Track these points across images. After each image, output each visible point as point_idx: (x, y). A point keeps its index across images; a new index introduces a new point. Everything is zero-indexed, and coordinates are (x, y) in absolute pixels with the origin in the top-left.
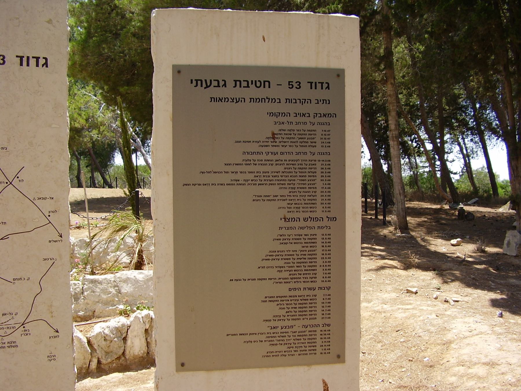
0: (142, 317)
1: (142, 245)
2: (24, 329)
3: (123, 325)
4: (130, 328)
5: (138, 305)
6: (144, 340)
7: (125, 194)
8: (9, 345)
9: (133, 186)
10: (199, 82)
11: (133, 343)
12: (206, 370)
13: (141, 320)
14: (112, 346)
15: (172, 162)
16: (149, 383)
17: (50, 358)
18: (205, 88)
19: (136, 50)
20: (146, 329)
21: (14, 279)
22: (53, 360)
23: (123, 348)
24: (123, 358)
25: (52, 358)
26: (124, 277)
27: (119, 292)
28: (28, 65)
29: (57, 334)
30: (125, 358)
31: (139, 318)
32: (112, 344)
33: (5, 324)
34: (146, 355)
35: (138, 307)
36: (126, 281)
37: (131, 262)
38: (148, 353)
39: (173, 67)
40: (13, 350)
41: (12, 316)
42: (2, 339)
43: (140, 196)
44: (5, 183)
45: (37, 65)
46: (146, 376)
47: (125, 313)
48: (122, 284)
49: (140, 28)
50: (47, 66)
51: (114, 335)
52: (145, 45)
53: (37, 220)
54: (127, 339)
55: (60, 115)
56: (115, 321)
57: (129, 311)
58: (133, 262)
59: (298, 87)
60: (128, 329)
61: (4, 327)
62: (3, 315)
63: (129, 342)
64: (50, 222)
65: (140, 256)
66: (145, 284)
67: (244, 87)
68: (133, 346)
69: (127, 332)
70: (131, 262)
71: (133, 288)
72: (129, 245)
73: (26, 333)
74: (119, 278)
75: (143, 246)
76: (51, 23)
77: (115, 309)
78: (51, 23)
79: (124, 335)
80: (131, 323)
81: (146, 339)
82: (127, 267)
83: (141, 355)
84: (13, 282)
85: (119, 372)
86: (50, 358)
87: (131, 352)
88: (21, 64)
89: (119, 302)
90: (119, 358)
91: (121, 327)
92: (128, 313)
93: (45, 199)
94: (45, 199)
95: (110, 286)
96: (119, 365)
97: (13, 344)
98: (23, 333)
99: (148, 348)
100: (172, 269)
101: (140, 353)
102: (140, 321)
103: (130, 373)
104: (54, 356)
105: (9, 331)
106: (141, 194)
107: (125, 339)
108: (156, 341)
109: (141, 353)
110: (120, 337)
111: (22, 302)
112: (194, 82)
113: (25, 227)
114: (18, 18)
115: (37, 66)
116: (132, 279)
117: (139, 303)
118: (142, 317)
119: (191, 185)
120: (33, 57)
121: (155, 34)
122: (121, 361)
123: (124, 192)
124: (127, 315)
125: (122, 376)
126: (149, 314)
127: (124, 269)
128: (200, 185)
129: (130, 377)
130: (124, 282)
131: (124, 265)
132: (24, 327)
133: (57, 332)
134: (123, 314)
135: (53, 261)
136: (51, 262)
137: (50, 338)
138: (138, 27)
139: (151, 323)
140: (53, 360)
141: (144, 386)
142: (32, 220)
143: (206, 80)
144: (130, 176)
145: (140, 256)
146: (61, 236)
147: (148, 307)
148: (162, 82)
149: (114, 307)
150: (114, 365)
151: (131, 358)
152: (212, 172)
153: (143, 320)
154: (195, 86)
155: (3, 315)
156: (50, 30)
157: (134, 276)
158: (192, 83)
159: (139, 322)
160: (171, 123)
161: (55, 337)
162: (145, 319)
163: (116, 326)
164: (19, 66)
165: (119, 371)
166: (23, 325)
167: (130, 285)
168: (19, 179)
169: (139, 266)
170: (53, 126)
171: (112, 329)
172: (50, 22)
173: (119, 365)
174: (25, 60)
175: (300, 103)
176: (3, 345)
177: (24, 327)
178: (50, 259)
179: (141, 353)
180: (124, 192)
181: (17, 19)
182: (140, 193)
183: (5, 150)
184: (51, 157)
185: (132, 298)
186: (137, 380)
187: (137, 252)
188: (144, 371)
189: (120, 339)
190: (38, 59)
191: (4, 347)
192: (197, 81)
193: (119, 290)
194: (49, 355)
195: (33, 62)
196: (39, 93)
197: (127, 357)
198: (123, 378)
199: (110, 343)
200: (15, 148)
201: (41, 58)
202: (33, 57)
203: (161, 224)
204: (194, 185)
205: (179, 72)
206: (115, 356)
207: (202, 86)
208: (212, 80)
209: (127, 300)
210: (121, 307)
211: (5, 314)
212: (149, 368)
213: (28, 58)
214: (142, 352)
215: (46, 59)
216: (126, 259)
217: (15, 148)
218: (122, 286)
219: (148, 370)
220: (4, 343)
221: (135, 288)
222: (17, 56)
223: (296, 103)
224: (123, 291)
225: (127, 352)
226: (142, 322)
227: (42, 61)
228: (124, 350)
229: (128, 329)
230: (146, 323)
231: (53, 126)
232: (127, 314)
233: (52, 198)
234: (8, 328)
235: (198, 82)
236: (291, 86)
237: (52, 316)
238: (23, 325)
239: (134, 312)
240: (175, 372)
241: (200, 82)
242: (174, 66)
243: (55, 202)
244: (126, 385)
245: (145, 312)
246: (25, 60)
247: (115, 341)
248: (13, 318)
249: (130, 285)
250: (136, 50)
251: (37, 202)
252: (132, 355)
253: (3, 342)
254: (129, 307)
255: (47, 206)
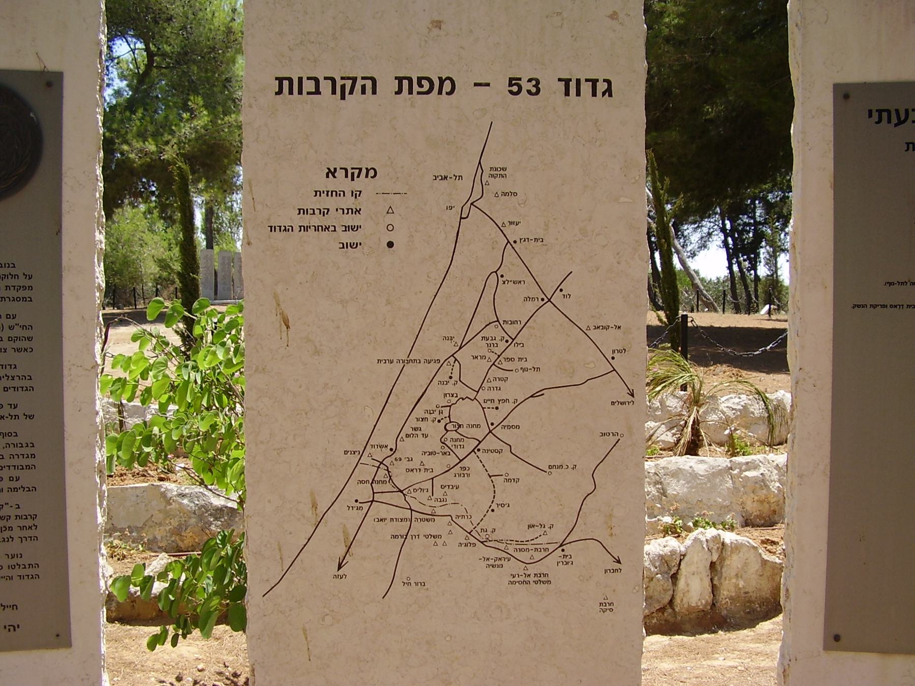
0: (707, 541)
1: (698, 412)
2: (563, 553)
3: (673, 552)
4: (686, 558)
5: (697, 519)
6: (707, 582)
7: (660, 320)
8: (536, 579)
9: (673, 307)
10: (885, 115)
11: (688, 585)
12: (879, 652)
13: (705, 546)
14: (652, 588)
15: (832, 264)
16: (717, 659)
17: (603, 608)
18: (896, 125)
19: (670, 67)
20: (711, 563)
21: (550, 467)
22: (608, 611)
23: (671, 592)
24: (670, 610)
25: (608, 607)
26: (672, 467)
27: (664, 493)
28: (578, 94)
29: (617, 566)
30: (674, 610)
31: (701, 542)
32: (652, 584)
33: (533, 542)
34: (709, 607)
35: (697, 521)
36: (676, 473)
37: (679, 440)
38: (714, 604)
39: (834, 88)
40: (541, 588)
41: (544, 529)
42: (526, 569)
43: (690, 324)
44: (540, 300)
45: (594, 94)
46: (711, 645)
47: (671, 531)
48: (667, 480)
49: (678, 27)
50: (610, 95)
51: (656, 568)
52: (687, 58)
53: (592, 365)
54: (678, 576)
55: (633, 181)
56: (659, 545)
57: (681, 527)
58: (682, 442)
59: (534, 90)
60: (681, 560)
61: (530, 547)
62: (529, 527)
63: (681, 583)
64: (614, 370)
65: (696, 432)
66: (709, 481)
67: (308, 93)
68: (688, 591)
69: (680, 564)
70: (679, 440)
71: (688, 488)
72: (671, 411)
73: (566, 560)
74: (663, 468)
75: (700, 413)
76: (617, 19)
77: (655, 522)
78: (617, 19)
79: (673, 571)
80: (687, 548)
81: (712, 580)
82: (670, 449)
83: (701, 607)
84: (548, 470)
85: (662, 634)
86: (603, 608)
87: (685, 600)
88: (567, 93)
89: (663, 511)
90: (662, 610)
91: (668, 556)
92: (678, 530)
93: (606, 328)
94: (606, 328)
95: (648, 482)
96: (663, 622)
97: (543, 579)
98: (560, 560)
99: (714, 595)
100: (827, 461)
101: (699, 604)
102: (703, 548)
103: (681, 637)
104: (610, 604)
105: (538, 556)
106: (692, 321)
107: (674, 577)
108: (787, 590)
109: (702, 603)
110: (666, 573)
111: (561, 507)
112: (875, 115)
113: (571, 377)
114: (561, 13)
115: (593, 96)
116: (687, 471)
117: (698, 515)
118: (707, 541)
119: (869, 306)
120: (587, 80)
121: (799, 29)
122: (666, 615)
123: (658, 316)
124: (676, 535)
125: (668, 642)
126: (719, 535)
127: (661, 452)
128: (884, 306)
129: (682, 646)
130: (672, 477)
131: (661, 445)
132: (563, 550)
133: (619, 562)
134: (670, 533)
135: (617, 438)
136: (613, 439)
137: (606, 571)
138: (675, 26)
139: (722, 552)
140: (608, 611)
141: (709, 662)
142: (584, 365)
143: (897, 111)
144: (669, 288)
145: (696, 432)
146: (632, 395)
147: (713, 523)
148: (813, 117)
149: (654, 519)
150: (654, 621)
151: (683, 611)
152: (909, 284)
153: (707, 546)
154: (877, 123)
155: (529, 527)
156: (614, 31)
157: (691, 467)
158: (870, 115)
159: (701, 549)
160: (831, 193)
161: (615, 571)
162: (711, 545)
163: (661, 553)
164: (564, 95)
165: (663, 633)
166: (560, 546)
167: (682, 482)
168: (563, 293)
169: (693, 448)
170: (622, 199)
171: (654, 558)
172: (614, 16)
173: (663, 622)
174: (573, 85)
175: (334, 92)
176: (527, 579)
177: (563, 550)
178: (611, 434)
179: (702, 603)
180: (658, 316)
181: (559, 14)
182: (689, 320)
183: (540, 243)
184: (618, 254)
185: (685, 505)
186: (696, 652)
187: (691, 423)
188: (706, 636)
189: (666, 576)
190: (594, 82)
191: (528, 583)
192: (880, 112)
193: (663, 489)
194: (603, 601)
195: (586, 88)
196: (598, 143)
197: (677, 610)
198: (670, 645)
199: (649, 581)
200: (557, 239)
201: (601, 80)
202: (587, 80)
203: (810, 378)
204: (874, 306)
205: (846, 97)
206: (656, 606)
207: (889, 121)
208: (910, 111)
209: (676, 509)
210: (668, 520)
211: (533, 526)
212: (714, 632)
213: (578, 81)
214: (704, 602)
215: (609, 82)
216: (669, 437)
217: (557, 239)
218: (669, 484)
219: (713, 635)
220: (529, 575)
221: (692, 488)
222: (560, 80)
223: (317, 92)
224: (670, 491)
225: (678, 601)
226: (706, 549)
227: (601, 87)
228: (673, 597)
229: (681, 560)
230: (713, 551)
231: (622, 199)
232: (676, 532)
233: (619, 327)
234: (536, 549)
235: (881, 115)
236: (515, 89)
237: (611, 535)
238: (560, 546)
239: (689, 530)
240: (821, 649)
241: (886, 113)
242: (837, 87)
243: (624, 333)
244: (676, 658)
245: (711, 532)
246: (573, 85)
247: (658, 580)
248: (545, 533)
249: (682, 482)
250: (670, 67)
251: (593, 334)
252: (686, 606)
253: (528, 573)
254: (681, 521)
255: (609, 341)
